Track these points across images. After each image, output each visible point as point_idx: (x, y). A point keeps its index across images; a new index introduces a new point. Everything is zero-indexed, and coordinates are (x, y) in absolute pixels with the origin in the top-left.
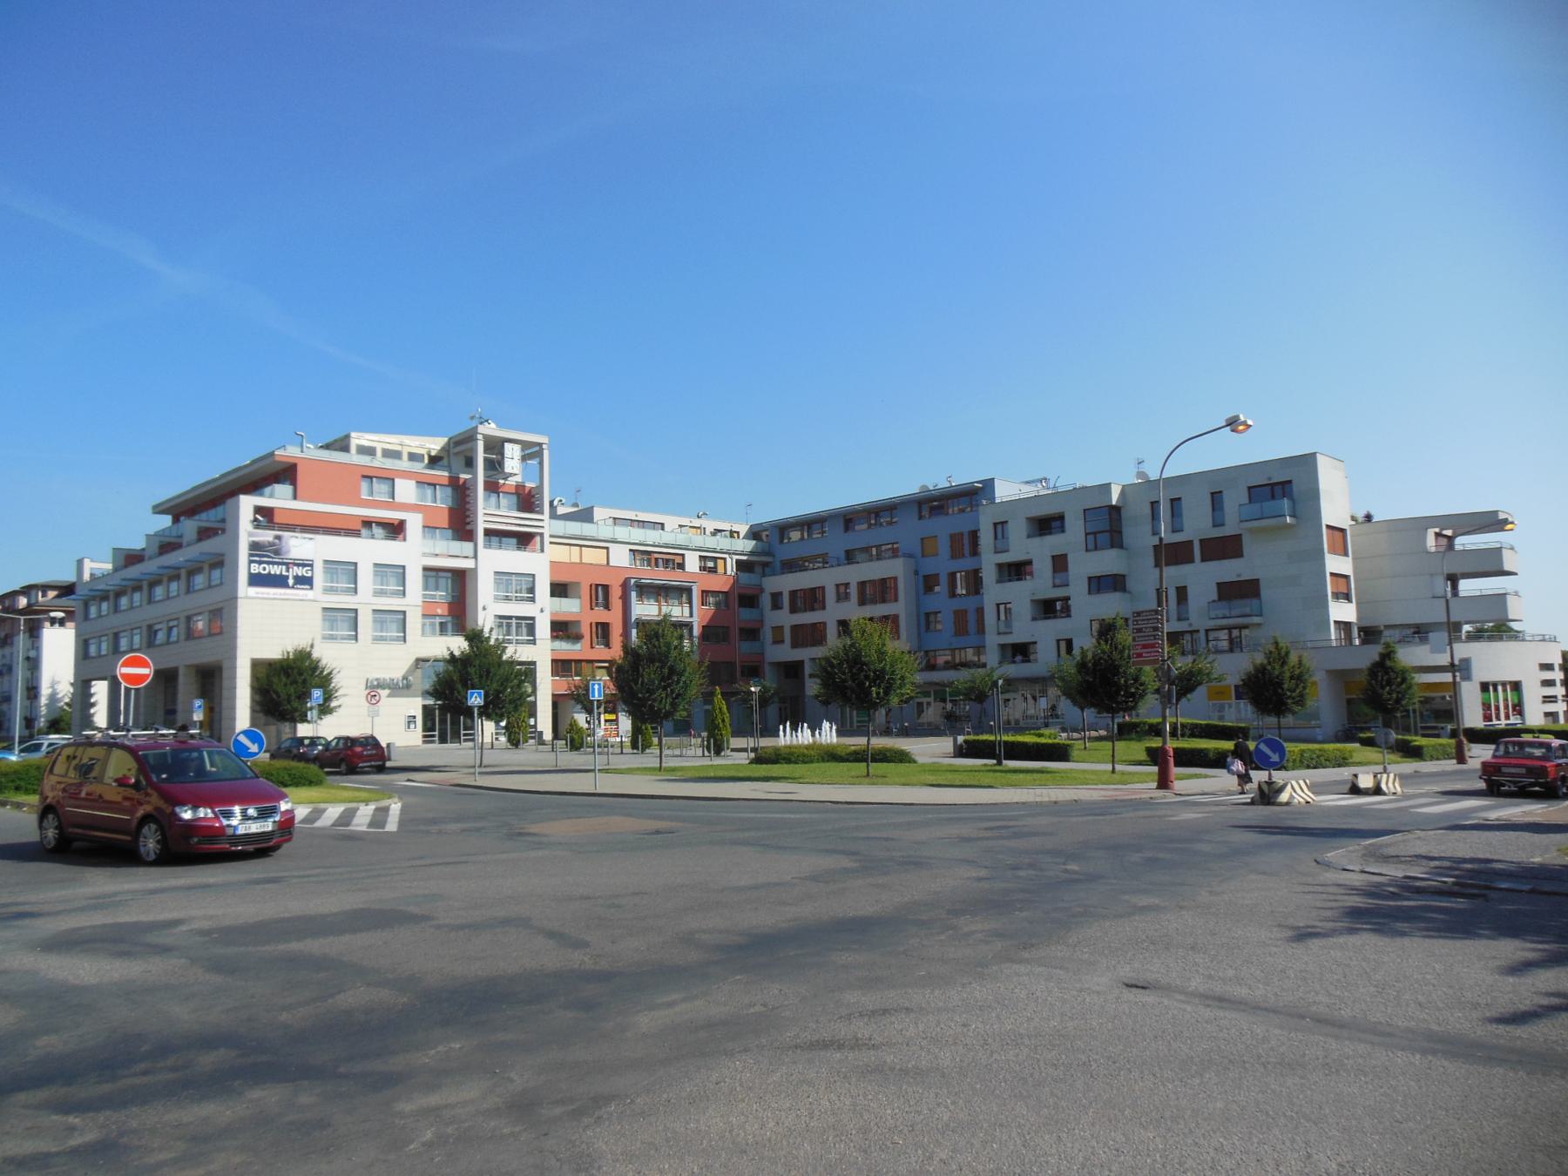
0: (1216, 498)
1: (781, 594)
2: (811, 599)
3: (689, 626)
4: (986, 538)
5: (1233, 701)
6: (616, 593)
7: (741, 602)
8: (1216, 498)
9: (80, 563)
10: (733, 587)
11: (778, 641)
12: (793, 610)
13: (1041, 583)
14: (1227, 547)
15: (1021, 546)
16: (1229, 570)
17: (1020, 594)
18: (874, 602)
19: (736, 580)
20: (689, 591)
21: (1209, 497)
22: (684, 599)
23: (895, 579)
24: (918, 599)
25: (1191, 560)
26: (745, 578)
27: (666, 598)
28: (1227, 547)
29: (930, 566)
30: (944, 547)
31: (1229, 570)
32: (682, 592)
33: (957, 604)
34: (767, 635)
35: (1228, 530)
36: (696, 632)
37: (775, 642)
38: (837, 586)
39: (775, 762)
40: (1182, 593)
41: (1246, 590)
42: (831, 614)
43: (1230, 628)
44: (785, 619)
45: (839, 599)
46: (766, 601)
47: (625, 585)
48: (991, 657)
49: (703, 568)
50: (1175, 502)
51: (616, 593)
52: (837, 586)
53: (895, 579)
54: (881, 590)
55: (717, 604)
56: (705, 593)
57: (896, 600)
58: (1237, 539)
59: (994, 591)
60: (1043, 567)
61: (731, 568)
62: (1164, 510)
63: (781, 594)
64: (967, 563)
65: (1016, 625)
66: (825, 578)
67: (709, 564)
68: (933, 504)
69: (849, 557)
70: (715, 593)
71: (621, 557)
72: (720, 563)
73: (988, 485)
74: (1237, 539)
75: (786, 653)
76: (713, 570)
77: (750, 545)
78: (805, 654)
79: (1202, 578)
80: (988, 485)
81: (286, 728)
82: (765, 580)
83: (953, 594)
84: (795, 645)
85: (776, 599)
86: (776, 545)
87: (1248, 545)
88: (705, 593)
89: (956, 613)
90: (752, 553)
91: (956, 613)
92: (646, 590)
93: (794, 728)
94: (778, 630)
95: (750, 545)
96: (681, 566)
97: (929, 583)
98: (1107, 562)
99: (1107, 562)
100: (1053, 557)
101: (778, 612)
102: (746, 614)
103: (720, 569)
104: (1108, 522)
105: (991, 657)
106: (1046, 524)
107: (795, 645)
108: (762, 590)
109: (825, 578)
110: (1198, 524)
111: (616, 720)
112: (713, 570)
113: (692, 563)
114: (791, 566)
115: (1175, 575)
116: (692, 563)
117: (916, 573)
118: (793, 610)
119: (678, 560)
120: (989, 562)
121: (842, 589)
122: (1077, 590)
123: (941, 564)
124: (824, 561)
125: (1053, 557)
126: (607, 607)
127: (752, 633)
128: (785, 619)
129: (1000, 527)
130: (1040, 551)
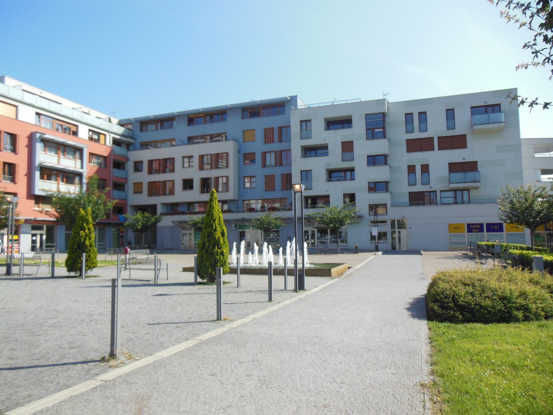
0: (450, 114)
1: (141, 162)
2: (166, 165)
3: (80, 175)
4: (295, 129)
5: (466, 233)
6: (22, 143)
7: (113, 168)
8: (450, 114)
10: (110, 154)
12: (150, 172)
13: (334, 159)
14: (458, 142)
15: (319, 135)
16: (457, 155)
17: (318, 165)
18: (158, 172)
19: (112, 152)
20: (81, 150)
21: (445, 111)
22: (77, 155)
23: (227, 154)
24: (239, 168)
25: (432, 149)
26: (118, 150)
27: (64, 152)
28: (458, 142)
29: (249, 148)
30: (260, 136)
31: (457, 155)
32: (77, 151)
33: (268, 171)
34: (130, 187)
35: (457, 132)
37: (136, 192)
40: (425, 168)
41: (471, 167)
42: (178, 176)
43: (455, 191)
44: (145, 177)
46: (130, 166)
47: (31, 138)
49: (91, 139)
50: (423, 115)
51: (22, 143)
53: (227, 154)
54: (217, 160)
56: (92, 155)
57: (227, 167)
58: (464, 137)
59: (298, 164)
60: (335, 150)
61: (109, 142)
62: (418, 170)
63: (141, 162)
64: (277, 146)
65: (314, 185)
66: (176, 152)
67: (96, 135)
68: (252, 111)
69: (191, 140)
71: (27, 115)
72: (102, 137)
73: (294, 99)
74: (464, 137)
75: (144, 199)
76: (98, 141)
77: (121, 130)
78: (158, 201)
79: (439, 160)
80: (294, 99)
81: (120, 216)
82: (130, 153)
83: (264, 165)
84: (150, 194)
85: (138, 167)
86: (141, 131)
87: (469, 141)
88: (92, 155)
90: (122, 135)
92: (49, 144)
95: (121, 130)
96: (75, 133)
97: (248, 158)
98: (378, 147)
99: (378, 147)
100: (343, 143)
102: (117, 173)
103: (102, 141)
104: (377, 122)
106: (333, 124)
107: (150, 194)
108: (128, 160)
109: (176, 152)
110: (437, 127)
111: (18, 241)
112: (98, 141)
113: (84, 133)
114: (145, 145)
115: (418, 158)
116: (84, 133)
117: (239, 152)
118: (150, 172)
119: (73, 129)
120: (296, 145)
122: (359, 162)
123: (258, 146)
124: (171, 142)
125: (343, 143)
126: (14, 150)
127: (119, 186)
128: (145, 177)
129: (305, 123)
130: (334, 139)
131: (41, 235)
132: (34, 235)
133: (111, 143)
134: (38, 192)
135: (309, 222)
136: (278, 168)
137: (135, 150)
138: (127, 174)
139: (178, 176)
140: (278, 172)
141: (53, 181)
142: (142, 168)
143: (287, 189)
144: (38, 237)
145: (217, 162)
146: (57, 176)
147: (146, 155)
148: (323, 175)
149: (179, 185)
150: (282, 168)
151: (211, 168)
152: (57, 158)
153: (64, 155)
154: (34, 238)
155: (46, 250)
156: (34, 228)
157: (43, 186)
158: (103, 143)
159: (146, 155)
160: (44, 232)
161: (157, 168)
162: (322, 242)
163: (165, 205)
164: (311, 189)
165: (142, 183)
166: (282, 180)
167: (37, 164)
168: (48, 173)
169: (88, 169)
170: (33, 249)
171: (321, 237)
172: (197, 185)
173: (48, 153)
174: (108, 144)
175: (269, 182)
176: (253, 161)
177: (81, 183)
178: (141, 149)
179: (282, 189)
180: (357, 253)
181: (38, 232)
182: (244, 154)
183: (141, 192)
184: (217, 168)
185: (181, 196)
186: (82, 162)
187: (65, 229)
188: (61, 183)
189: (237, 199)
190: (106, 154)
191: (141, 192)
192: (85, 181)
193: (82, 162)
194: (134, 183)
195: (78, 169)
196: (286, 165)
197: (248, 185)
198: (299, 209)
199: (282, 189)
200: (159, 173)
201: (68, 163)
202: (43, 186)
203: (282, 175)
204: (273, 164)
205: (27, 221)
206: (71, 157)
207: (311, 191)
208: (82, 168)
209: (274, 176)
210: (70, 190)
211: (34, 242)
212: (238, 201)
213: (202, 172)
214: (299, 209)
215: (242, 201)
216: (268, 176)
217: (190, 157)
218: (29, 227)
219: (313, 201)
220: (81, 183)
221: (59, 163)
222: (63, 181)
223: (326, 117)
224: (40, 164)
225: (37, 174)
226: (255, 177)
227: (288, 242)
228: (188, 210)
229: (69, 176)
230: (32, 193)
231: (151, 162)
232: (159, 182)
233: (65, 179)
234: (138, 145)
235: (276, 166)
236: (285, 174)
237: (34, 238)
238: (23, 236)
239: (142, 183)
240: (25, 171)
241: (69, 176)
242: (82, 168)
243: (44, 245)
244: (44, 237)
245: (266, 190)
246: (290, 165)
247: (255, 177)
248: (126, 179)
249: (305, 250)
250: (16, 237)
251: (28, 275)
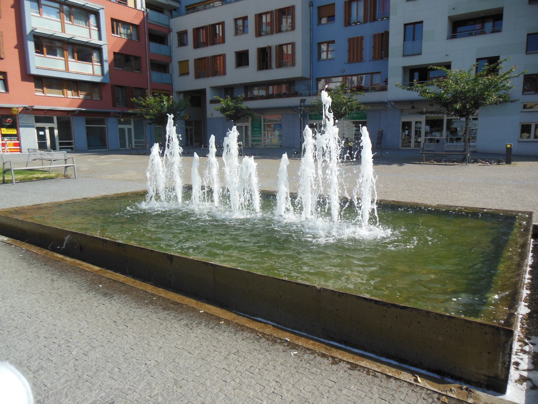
1: (185, 32)
2: (210, 35)
3: (99, 49)
9: (101, 98)
10: (143, 21)
11: (184, 73)
12: (197, 45)
18: (206, 44)
19: (146, 18)
22: (92, 19)
24: (311, 30)
26: (154, 16)
33: (354, 32)
34: (175, 67)
36: (107, 55)
37: (182, 74)
38: (236, 20)
39: (374, 8)
42: (229, 47)
44: (190, 53)
45: (237, 32)
46: (173, 39)
48: (395, 78)
52: (236, 20)
55: (129, 36)
57: (293, 28)
63: (185, 32)
65: (426, 46)
70: (126, 24)
75: (190, 83)
78: (207, 83)
83: (348, 23)
85: (182, 36)
89: (351, 41)
91: (351, 41)
93: (194, 142)
94: (184, 64)
101: (183, 48)
102: (155, 48)
105: (395, 78)
108: (170, 30)
111: (17, 136)
118: (197, 45)
121: (240, 22)
127: (162, 67)
128: (190, 53)
131: (51, 130)
132: (39, 129)
133: (144, 6)
134: (34, 71)
135: (413, 108)
136: (368, 24)
137: (180, 15)
138: (170, 52)
139: (229, 47)
140: (368, 31)
141: (58, 57)
142: (187, 42)
143: (382, 58)
144: (47, 131)
145: (280, 23)
146: (63, 49)
147: (189, 22)
148: (443, 27)
149: (231, 61)
150: (374, 24)
151: (272, 33)
152: (59, 24)
153: (70, 20)
154: (41, 133)
155: (61, 148)
156: (38, 120)
157: (41, 64)
158: (133, 6)
159: (189, 22)
160: (55, 125)
161: (205, 40)
162: (431, 140)
163: (217, 89)
164: (421, 54)
165: (188, 61)
166: (375, 44)
167: (28, 31)
168: (47, 44)
169: (110, 43)
170: (42, 146)
171: (431, 132)
172: (253, 58)
173: (45, 15)
174: (139, 7)
175: (355, 48)
176: (331, 18)
177: (101, 61)
178: (188, 13)
179: (374, 58)
180: (508, 162)
181: (47, 125)
182: (319, 8)
183: (188, 73)
184: (279, 31)
185: (234, 76)
186: (99, 31)
187: (84, 122)
188: (70, 59)
189: (307, 76)
190: (137, 22)
191: (188, 73)
192: (105, 56)
193: (99, 31)
194: (179, 62)
195: (95, 40)
196: (382, 19)
197: (324, 56)
198: (396, 90)
199: (374, 58)
200: (207, 46)
201: (79, 32)
202: (41, 64)
203: (375, 36)
204: (361, 19)
205: (26, 110)
206: (82, 23)
207: (419, 57)
208: (100, 38)
209: (362, 38)
210: (87, 71)
211: (41, 138)
212: (310, 79)
213: (260, 39)
214: (396, 90)
215: (315, 80)
216: (354, 39)
217: (245, 19)
218: (32, 119)
219: (419, 74)
220: (101, 61)
221: (63, 30)
222: (74, 58)
223: (446, 38)
224: (32, 31)
225: (31, 46)
226: (333, 42)
227: (308, 131)
228: (246, 94)
229: (84, 51)
230: (28, 73)
231: (197, 31)
232: (207, 58)
233: (76, 55)
234: (183, 10)
235: (365, 22)
236: (379, 34)
237: (41, 133)
238: (23, 131)
239: (188, 61)
240: (15, 42)
241: (84, 51)
242: (100, 38)
243: (57, 142)
244: (56, 132)
245: (350, 61)
246: (388, 18)
247: (333, 42)
248: (170, 58)
249: (367, 154)
250: (13, 132)
251: (30, 180)
